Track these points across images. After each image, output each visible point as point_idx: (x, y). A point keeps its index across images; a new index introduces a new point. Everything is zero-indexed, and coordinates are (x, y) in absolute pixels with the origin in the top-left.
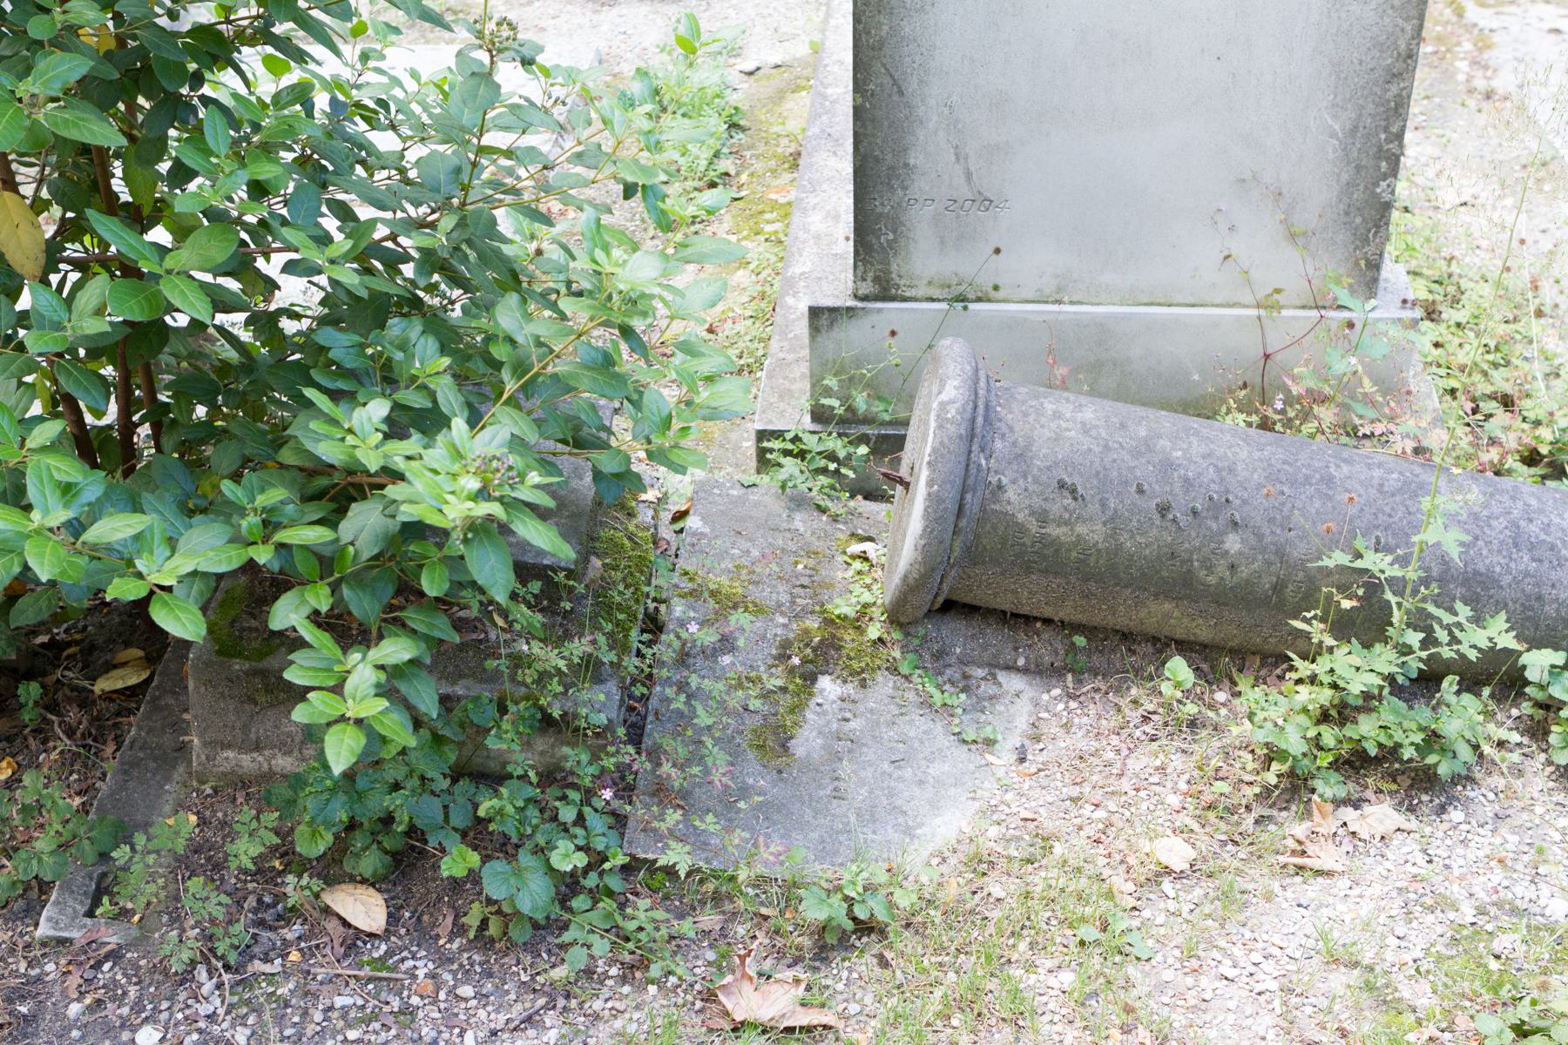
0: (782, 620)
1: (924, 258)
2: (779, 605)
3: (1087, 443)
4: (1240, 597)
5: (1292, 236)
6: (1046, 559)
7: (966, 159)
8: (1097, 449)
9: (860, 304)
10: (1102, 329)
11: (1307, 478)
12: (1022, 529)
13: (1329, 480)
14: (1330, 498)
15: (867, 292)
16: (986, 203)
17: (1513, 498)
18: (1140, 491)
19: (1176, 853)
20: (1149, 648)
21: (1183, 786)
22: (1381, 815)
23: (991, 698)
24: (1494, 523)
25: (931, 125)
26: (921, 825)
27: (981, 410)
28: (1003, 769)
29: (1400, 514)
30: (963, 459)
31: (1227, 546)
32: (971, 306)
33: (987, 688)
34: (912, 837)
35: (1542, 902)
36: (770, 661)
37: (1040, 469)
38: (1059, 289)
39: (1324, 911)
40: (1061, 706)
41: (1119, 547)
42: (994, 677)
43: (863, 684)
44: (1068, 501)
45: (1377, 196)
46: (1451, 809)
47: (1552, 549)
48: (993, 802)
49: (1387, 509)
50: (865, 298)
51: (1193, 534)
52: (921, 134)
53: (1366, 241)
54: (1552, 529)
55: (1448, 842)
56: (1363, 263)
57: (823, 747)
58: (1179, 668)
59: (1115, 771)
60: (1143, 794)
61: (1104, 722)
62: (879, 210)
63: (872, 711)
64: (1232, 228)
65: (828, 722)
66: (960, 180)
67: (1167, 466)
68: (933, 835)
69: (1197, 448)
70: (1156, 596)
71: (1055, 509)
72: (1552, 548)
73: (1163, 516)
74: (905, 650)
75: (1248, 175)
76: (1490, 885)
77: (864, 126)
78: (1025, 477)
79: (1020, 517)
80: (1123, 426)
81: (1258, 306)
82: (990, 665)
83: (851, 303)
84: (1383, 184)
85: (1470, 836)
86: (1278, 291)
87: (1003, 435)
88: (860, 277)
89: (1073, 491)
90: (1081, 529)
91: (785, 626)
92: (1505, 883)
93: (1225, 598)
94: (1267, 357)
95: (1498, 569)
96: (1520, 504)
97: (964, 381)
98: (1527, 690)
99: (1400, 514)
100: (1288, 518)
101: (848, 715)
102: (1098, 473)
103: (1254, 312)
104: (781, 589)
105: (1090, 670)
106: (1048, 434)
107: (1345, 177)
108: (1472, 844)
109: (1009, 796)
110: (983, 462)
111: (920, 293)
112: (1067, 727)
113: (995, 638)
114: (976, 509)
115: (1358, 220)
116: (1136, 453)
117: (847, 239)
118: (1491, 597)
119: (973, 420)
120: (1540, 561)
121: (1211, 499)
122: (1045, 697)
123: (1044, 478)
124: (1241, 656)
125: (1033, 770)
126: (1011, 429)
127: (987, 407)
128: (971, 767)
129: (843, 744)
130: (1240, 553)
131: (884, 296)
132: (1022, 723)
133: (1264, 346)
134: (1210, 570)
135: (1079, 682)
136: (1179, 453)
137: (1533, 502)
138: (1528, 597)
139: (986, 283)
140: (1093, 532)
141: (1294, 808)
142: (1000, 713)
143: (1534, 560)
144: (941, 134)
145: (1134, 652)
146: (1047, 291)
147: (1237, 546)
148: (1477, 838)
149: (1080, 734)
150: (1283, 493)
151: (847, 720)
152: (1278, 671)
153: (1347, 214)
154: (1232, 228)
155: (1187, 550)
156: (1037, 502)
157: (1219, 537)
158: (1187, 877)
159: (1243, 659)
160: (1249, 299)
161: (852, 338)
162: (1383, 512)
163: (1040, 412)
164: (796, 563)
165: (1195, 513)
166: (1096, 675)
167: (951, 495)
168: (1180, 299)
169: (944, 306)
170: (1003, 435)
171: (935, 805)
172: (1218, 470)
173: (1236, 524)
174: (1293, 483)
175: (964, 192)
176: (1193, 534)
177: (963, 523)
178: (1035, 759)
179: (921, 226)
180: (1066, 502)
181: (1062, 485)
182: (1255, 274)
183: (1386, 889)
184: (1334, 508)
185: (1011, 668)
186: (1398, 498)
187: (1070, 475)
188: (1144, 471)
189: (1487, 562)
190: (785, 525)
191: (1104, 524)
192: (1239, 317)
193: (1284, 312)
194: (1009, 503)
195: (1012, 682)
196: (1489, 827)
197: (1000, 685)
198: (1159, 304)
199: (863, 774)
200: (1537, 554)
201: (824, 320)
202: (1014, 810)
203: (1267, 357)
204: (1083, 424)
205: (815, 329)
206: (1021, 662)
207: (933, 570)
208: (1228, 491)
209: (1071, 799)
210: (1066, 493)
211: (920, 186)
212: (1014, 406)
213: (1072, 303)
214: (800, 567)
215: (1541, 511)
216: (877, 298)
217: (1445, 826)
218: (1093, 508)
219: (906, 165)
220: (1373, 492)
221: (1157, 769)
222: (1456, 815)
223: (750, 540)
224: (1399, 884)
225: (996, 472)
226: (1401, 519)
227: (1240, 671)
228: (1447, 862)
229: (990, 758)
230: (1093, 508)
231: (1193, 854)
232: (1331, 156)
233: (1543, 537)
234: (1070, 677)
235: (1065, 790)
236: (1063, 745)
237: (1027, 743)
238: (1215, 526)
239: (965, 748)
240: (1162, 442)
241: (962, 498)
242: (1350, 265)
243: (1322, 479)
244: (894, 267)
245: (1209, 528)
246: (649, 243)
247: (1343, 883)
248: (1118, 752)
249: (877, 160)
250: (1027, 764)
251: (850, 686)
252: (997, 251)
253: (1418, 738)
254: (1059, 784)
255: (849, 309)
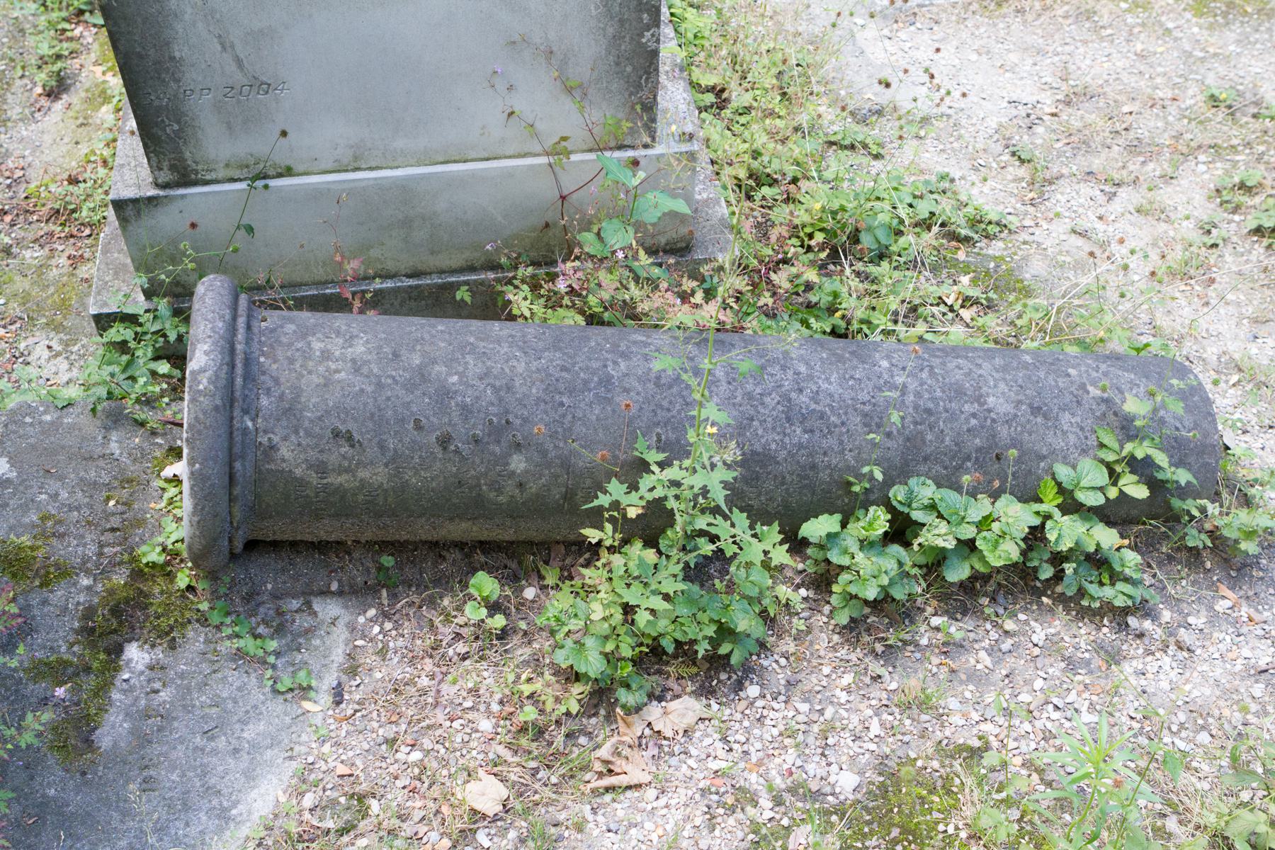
0: (85, 581)
1: (215, 143)
2: (85, 560)
3: (359, 383)
4: (537, 507)
5: (569, 90)
6: (338, 504)
7: (232, 46)
8: (369, 389)
9: (161, 193)
10: (404, 189)
11: (586, 382)
12: (302, 483)
13: (607, 381)
14: (609, 401)
15: (167, 179)
16: (262, 86)
17: (784, 368)
18: (418, 426)
19: (486, 794)
20: (455, 555)
21: (495, 707)
22: (683, 709)
23: (307, 631)
24: (767, 400)
25: (187, 17)
26: (235, 804)
27: (239, 365)
28: (320, 716)
29: (678, 407)
30: (223, 431)
31: (512, 466)
32: (273, 183)
33: (302, 621)
34: (228, 819)
35: (832, 779)
36: (72, 638)
37: (311, 421)
38: (356, 158)
39: (633, 831)
40: (376, 629)
41: (405, 485)
42: (310, 607)
43: (173, 646)
44: (345, 449)
45: (644, 46)
46: (747, 683)
47: (822, 418)
48: (310, 760)
49: (665, 404)
50: (165, 186)
51: (478, 461)
52: (179, 27)
53: (639, 87)
54: (821, 396)
55: (746, 723)
56: (638, 108)
57: (132, 732)
58: (485, 584)
59: (430, 700)
60: (456, 724)
61: (419, 642)
62: (156, 103)
63: (182, 676)
64: (510, 88)
65: (137, 699)
66: (232, 67)
67: (445, 394)
68: (250, 813)
69: (473, 366)
70: (451, 519)
71: (333, 459)
72: (822, 416)
73: (445, 449)
74: (215, 596)
75: (517, 38)
76: (785, 767)
77: (116, 24)
78: (297, 432)
79: (298, 472)
80: (396, 355)
81: (548, 154)
82: (303, 593)
83: (152, 192)
84: (648, 34)
85: (765, 712)
86: (564, 139)
87: (269, 389)
88: (155, 167)
89: (349, 438)
90: (363, 474)
91: (89, 588)
92: (799, 763)
93: (514, 512)
94: (563, 198)
95: (773, 446)
96: (790, 373)
97: (215, 343)
98: (809, 551)
99: (678, 407)
100: (570, 429)
101: (157, 685)
102: (372, 415)
103: (543, 160)
104: (88, 538)
105: (403, 582)
106: (315, 379)
107: (610, 31)
108: (768, 722)
109: (326, 748)
110: (250, 424)
111: (221, 174)
112: (382, 653)
113: (304, 566)
114: (250, 471)
115: (629, 69)
116: (410, 387)
117: (133, 133)
118: (769, 473)
119: (231, 381)
120: (812, 431)
121: (491, 422)
122: (361, 619)
123: (317, 429)
124: (544, 549)
125: (350, 712)
126: (277, 381)
127: (247, 362)
128: (288, 720)
129: (152, 724)
130: (527, 471)
131: (185, 177)
132: (338, 655)
133: (560, 188)
134: (499, 491)
135: (394, 597)
136: (456, 378)
137: (803, 369)
138: (803, 468)
139: (281, 159)
140: (376, 475)
141: (602, 712)
142: (316, 648)
143: (805, 431)
144: (200, 25)
145: (444, 558)
146: (345, 161)
147: (522, 466)
148: (772, 714)
149: (396, 660)
150: (562, 404)
151: (157, 692)
152: (582, 560)
153: (617, 64)
154: (510, 88)
155: (472, 477)
156: (313, 455)
157: (504, 460)
158: (501, 819)
159: (549, 549)
160: (538, 149)
161: (169, 221)
162: (661, 407)
163: (307, 355)
164: (108, 499)
165: (477, 441)
166: (410, 586)
167: (216, 473)
168: (473, 155)
169: (242, 186)
170: (269, 389)
171: (250, 776)
172: (496, 390)
173: (519, 444)
174: (571, 391)
175: (239, 78)
176: (478, 461)
177: (237, 491)
178: (353, 696)
179: (202, 109)
180: (343, 450)
181: (336, 434)
182: (540, 126)
183: (690, 793)
184: (614, 411)
185: (325, 593)
186: (675, 390)
187: (344, 422)
188: (421, 404)
189: (763, 441)
190: (99, 451)
191: (386, 465)
192: (531, 167)
193: (574, 158)
194: (283, 460)
195: (328, 609)
196: (782, 698)
197: (315, 614)
198: (455, 162)
199: (173, 755)
200: (808, 425)
201: (129, 211)
202: (331, 765)
203: (563, 198)
204: (354, 361)
205: (123, 220)
206: (334, 586)
207: (215, 540)
208: (507, 412)
209: (386, 741)
210: (342, 442)
211: (192, 77)
212: (280, 353)
213: (371, 169)
214: (112, 503)
215: (810, 377)
216: (179, 185)
217: (743, 704)
218: (372, 452)
219: (172, 58)
220: (651, 386)
221: (470, 691)
222: (753, 691)
223: (61, 478)
224: (701, 785)
225: (265, 432)
226: (679, 412)
227: (547, 563)
228: (745, 747)
229: (307, 705)
230: (372, 452)
231: (503, 792)
232: (594, 13)
233: (813, 406)
234: (384, 593)
235: (381, 732)
236: (381, 674)
237: (344, 678)
238: (497, 450)
239: (281, 698)
240: (437, 368)
241: (231, 467)
242: (627, 110)
243: (600, 381)
244: (187, 155)
245: (493, 454)
246: (18, 83)
247: (651, 793)
248: (432, 677)
249: (140, 56)
250: (343, 706)
251: (158, 650)
252: (284, 134)
253: (710, 631)
254: (375, 725)
255: (150, 200)
